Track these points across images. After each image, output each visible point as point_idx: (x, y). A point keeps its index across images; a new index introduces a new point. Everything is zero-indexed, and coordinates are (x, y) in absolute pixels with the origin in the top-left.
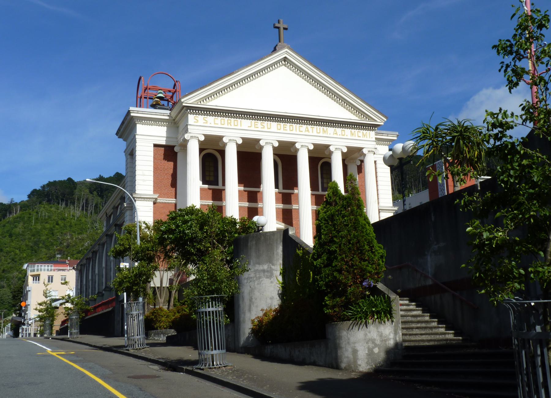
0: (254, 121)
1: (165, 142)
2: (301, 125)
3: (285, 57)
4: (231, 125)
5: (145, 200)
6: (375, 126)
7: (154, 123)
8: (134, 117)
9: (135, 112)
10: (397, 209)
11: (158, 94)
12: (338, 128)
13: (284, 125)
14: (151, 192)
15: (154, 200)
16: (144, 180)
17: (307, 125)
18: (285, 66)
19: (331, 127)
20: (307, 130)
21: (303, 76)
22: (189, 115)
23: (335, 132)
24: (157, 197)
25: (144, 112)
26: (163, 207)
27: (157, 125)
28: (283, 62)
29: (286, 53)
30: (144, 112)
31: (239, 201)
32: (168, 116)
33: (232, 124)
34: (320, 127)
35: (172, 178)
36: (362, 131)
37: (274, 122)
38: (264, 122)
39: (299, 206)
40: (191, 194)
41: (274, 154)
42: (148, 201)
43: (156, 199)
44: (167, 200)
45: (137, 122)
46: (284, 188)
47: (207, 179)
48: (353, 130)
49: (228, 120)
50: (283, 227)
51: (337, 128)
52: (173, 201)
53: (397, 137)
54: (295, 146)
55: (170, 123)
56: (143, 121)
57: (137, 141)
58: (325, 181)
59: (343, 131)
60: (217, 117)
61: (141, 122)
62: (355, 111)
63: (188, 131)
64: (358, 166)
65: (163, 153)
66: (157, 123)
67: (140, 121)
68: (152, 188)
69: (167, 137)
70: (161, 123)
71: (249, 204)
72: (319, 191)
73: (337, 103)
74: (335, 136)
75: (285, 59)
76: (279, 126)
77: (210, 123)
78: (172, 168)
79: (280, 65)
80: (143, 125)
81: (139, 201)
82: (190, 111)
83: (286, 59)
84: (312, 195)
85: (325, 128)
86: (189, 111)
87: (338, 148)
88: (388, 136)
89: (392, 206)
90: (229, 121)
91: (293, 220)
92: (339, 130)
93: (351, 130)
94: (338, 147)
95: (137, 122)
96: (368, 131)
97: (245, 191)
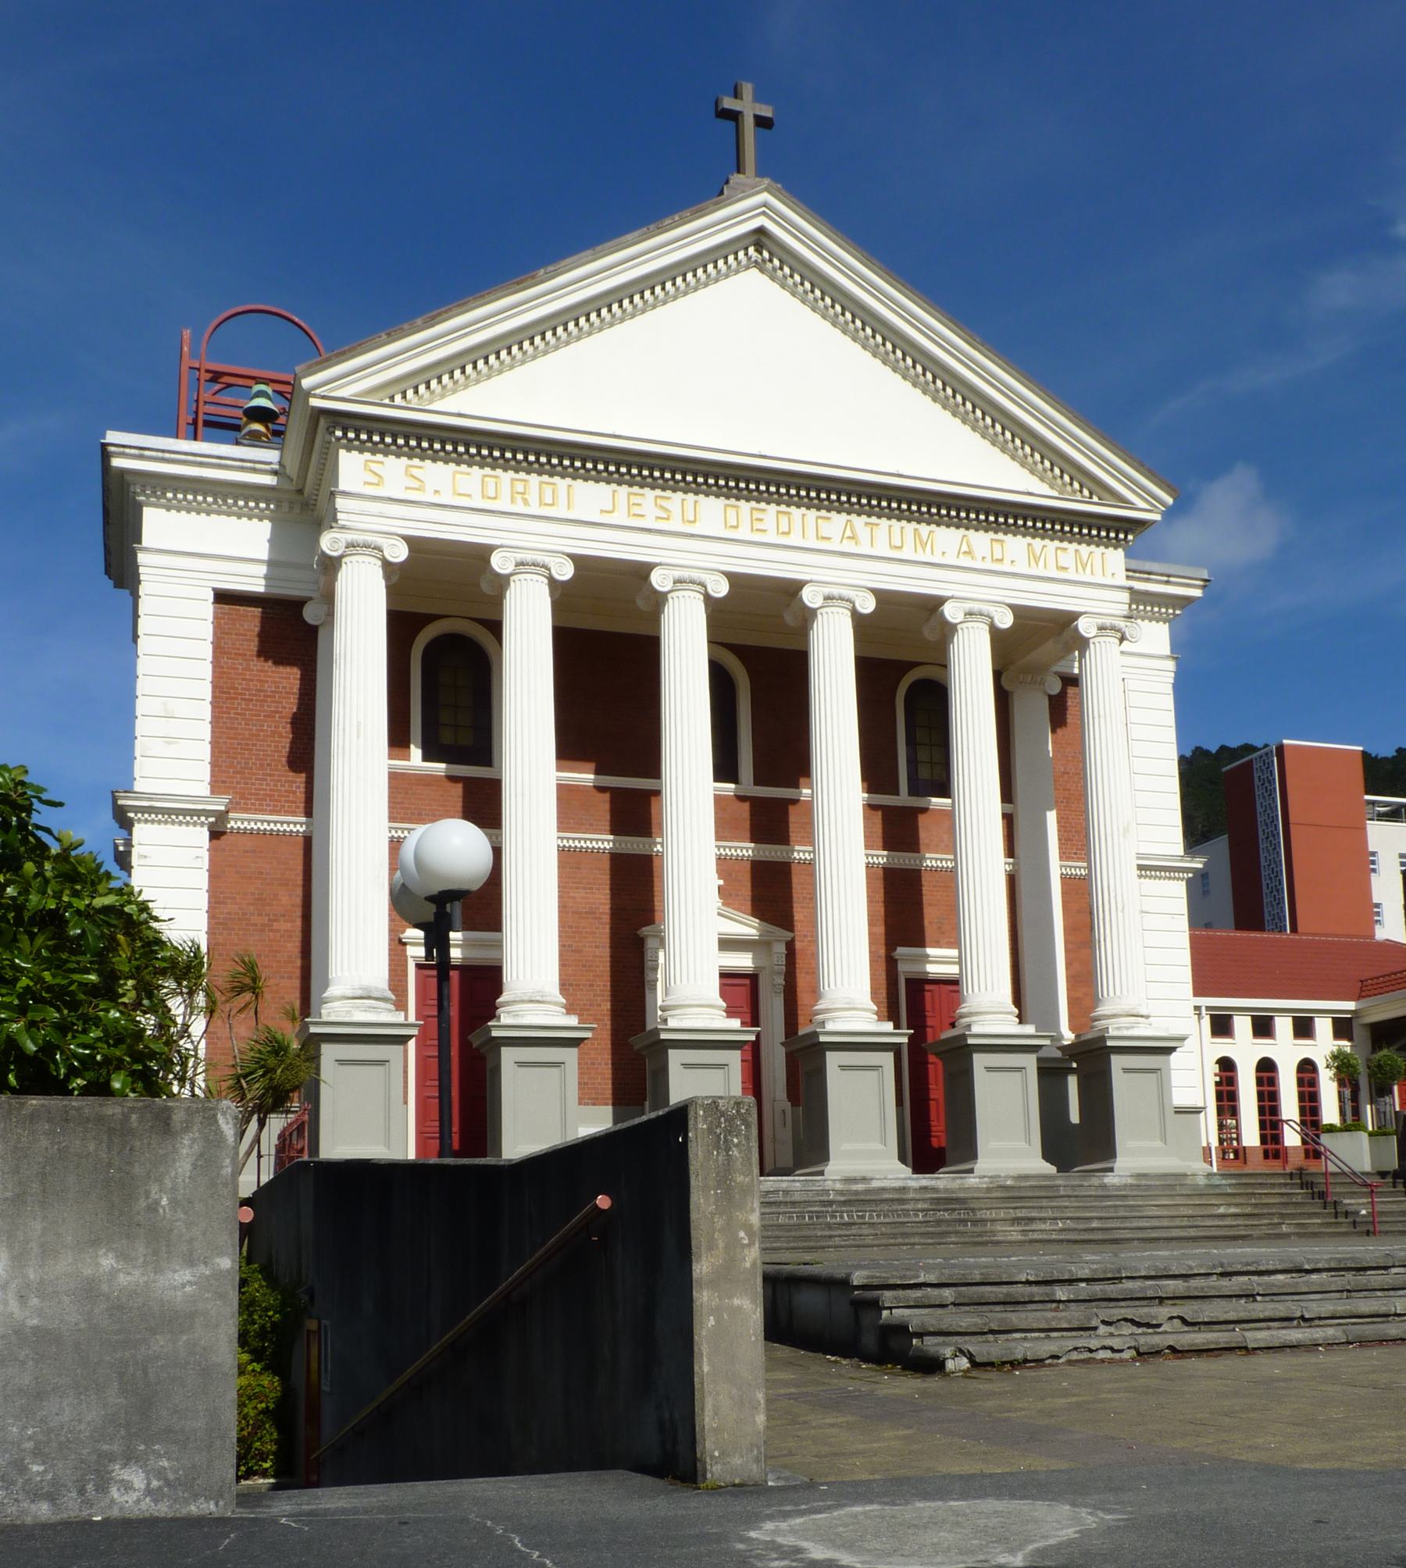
0: (625, 489)
1: (263, 582)
2: (823, 513)
3: (761, 231)
4: (526, 502)
5: (173, 822)
6: (1127, 526)
7: (215, 502)
8: (128, 478)
9: (127, 450)
10: (1200, 866)
11: (252, 399)
12: (977, 530)
13: (753, 509)
14: (204, 789)
15: (212, 820)
16: (169, 739)
17: (849, 513)
18: (762, 271)
19: (948, 526)
20: (848, 533)
21: (836, 315)
22: (342, 453)
23: (965, 548)
24: (222, 808)
25: (167, 455)
26: (253, 852)
27: (229, 515)
28: (751, 250)
29: (764, 213)
30: (167, 455)
31: (560, 829)
32: (275, 473)
33: (533, 496)
34: (904, 523)
35: (293, 732)
36: (1075, 545)
37: (712, 498)
38: (668, 493)
39: (814, 852)
40: (1109, 832)
41: (710, 642)
42: (188, 824)
43: (222, 816)
44: (269, 822)
45: (142, 498)
46: (758, 781)
47: (446, 737)
48: (1038, 543)
49: (513, 480)
50: (754, 932)
51: (972, 531)
52: (296, 824)
53: (1204, 587)
54: (801, 600)
55: (285, 507)
56: (170, 495)
57: (142, 577)
58: (923, 755)
59: (997, 546)
60: (464, 467)
61: (158, 498)
62: (1047, 464)
63: (336, 521)
64: (1050, 697)
65: (257, 629)
66: (230, 501)
67: (154, 492)
68: (204, 771)
69: (271, 563)
70: (257, 506)
71: (614, 842)
72: (898, 794)
73: (974, 429)
74: (965, 561)
75: (760, 238)
76: (731, 512)
77: (436, 492)
78: (296, 690)
79: (739, 263)
80: (168, 509)
81: (149, 825)
82: (345, 434)
83: (764, 240)
84: (870, 807)
85: (924, 529)
86: (339, 433)
87: (1108, 625)
88: (1167, 582)
89: (1182, 854)
90: (520, 487)
91: (795, 905)
92: (981, 541)
93: (1028, 539)
94: (976, 606)
95: (142, 498)
96: (1098, 546)
97: (600, 789)
